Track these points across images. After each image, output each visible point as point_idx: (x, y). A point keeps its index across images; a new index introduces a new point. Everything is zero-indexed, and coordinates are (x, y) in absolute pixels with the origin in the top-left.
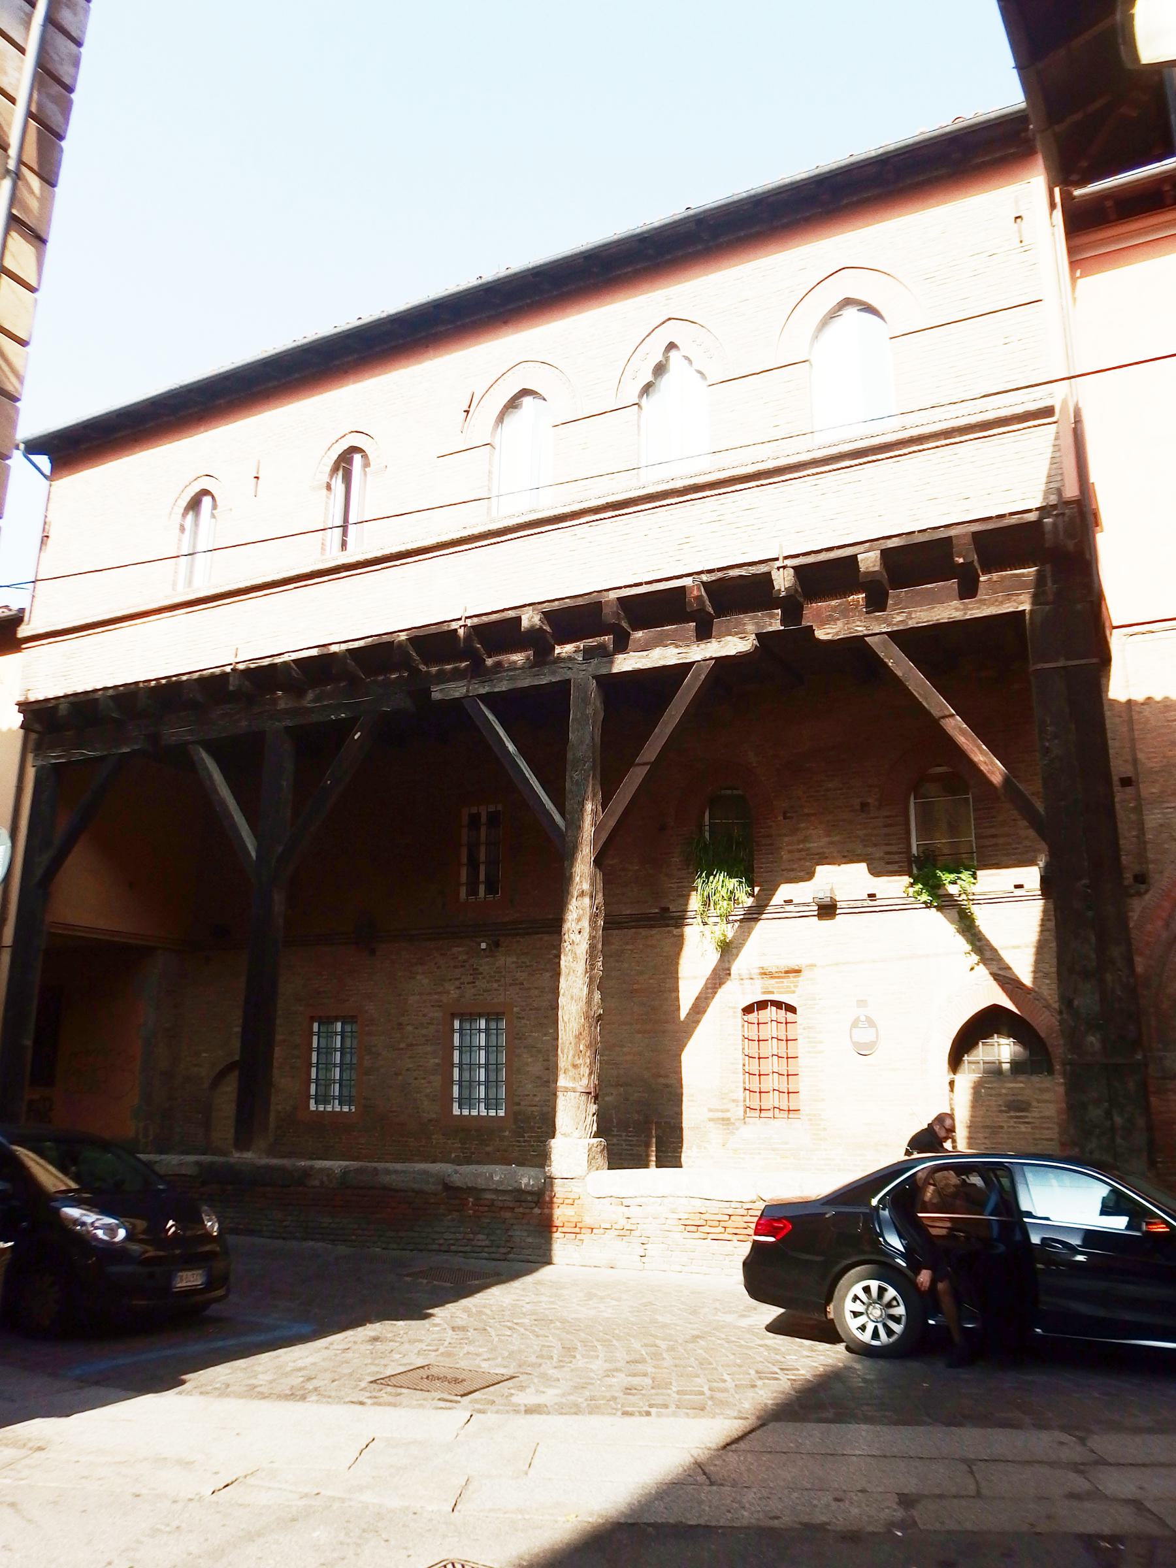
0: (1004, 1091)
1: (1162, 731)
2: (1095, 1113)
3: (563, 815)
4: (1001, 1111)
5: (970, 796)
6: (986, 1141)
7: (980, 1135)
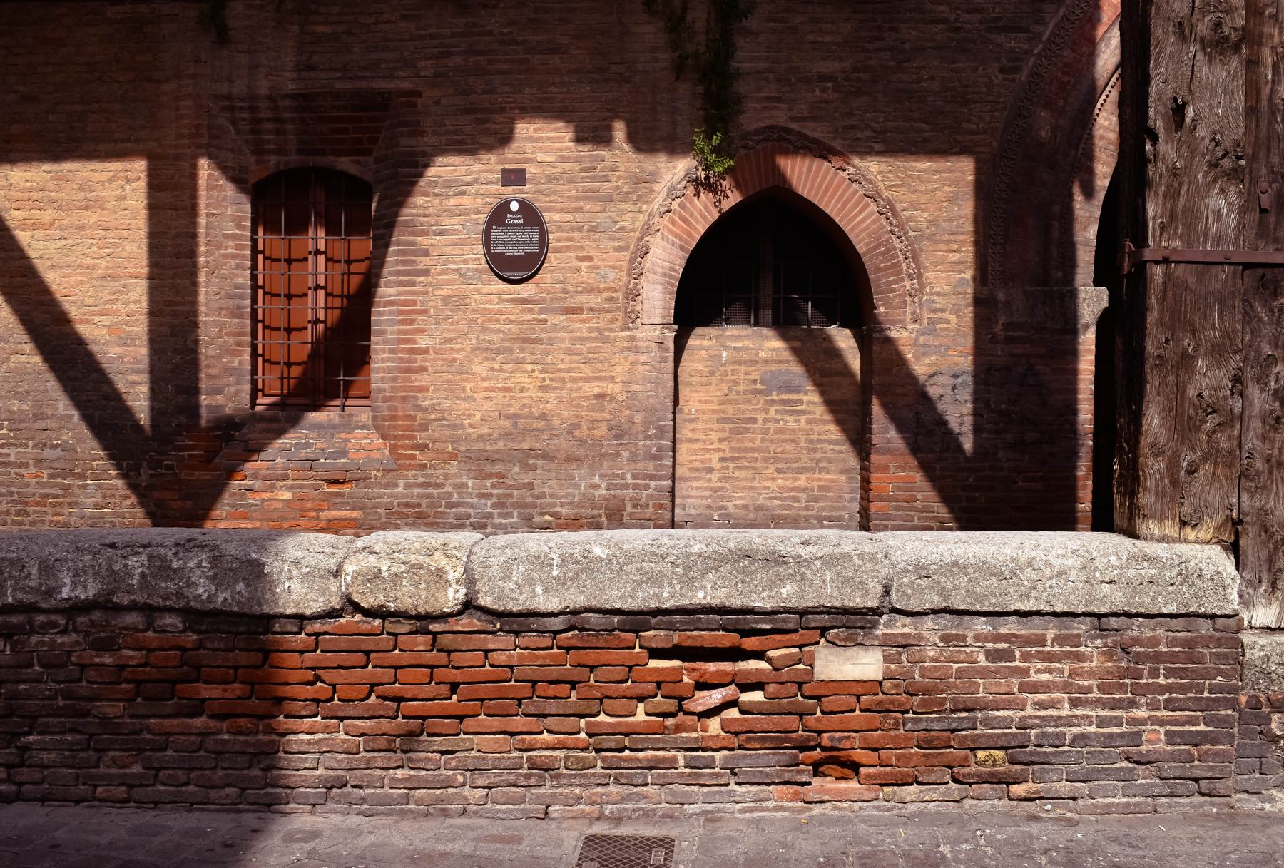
0: (763, 355)
4: (756, 392)
6: (724, 446)
7: (714, 436)
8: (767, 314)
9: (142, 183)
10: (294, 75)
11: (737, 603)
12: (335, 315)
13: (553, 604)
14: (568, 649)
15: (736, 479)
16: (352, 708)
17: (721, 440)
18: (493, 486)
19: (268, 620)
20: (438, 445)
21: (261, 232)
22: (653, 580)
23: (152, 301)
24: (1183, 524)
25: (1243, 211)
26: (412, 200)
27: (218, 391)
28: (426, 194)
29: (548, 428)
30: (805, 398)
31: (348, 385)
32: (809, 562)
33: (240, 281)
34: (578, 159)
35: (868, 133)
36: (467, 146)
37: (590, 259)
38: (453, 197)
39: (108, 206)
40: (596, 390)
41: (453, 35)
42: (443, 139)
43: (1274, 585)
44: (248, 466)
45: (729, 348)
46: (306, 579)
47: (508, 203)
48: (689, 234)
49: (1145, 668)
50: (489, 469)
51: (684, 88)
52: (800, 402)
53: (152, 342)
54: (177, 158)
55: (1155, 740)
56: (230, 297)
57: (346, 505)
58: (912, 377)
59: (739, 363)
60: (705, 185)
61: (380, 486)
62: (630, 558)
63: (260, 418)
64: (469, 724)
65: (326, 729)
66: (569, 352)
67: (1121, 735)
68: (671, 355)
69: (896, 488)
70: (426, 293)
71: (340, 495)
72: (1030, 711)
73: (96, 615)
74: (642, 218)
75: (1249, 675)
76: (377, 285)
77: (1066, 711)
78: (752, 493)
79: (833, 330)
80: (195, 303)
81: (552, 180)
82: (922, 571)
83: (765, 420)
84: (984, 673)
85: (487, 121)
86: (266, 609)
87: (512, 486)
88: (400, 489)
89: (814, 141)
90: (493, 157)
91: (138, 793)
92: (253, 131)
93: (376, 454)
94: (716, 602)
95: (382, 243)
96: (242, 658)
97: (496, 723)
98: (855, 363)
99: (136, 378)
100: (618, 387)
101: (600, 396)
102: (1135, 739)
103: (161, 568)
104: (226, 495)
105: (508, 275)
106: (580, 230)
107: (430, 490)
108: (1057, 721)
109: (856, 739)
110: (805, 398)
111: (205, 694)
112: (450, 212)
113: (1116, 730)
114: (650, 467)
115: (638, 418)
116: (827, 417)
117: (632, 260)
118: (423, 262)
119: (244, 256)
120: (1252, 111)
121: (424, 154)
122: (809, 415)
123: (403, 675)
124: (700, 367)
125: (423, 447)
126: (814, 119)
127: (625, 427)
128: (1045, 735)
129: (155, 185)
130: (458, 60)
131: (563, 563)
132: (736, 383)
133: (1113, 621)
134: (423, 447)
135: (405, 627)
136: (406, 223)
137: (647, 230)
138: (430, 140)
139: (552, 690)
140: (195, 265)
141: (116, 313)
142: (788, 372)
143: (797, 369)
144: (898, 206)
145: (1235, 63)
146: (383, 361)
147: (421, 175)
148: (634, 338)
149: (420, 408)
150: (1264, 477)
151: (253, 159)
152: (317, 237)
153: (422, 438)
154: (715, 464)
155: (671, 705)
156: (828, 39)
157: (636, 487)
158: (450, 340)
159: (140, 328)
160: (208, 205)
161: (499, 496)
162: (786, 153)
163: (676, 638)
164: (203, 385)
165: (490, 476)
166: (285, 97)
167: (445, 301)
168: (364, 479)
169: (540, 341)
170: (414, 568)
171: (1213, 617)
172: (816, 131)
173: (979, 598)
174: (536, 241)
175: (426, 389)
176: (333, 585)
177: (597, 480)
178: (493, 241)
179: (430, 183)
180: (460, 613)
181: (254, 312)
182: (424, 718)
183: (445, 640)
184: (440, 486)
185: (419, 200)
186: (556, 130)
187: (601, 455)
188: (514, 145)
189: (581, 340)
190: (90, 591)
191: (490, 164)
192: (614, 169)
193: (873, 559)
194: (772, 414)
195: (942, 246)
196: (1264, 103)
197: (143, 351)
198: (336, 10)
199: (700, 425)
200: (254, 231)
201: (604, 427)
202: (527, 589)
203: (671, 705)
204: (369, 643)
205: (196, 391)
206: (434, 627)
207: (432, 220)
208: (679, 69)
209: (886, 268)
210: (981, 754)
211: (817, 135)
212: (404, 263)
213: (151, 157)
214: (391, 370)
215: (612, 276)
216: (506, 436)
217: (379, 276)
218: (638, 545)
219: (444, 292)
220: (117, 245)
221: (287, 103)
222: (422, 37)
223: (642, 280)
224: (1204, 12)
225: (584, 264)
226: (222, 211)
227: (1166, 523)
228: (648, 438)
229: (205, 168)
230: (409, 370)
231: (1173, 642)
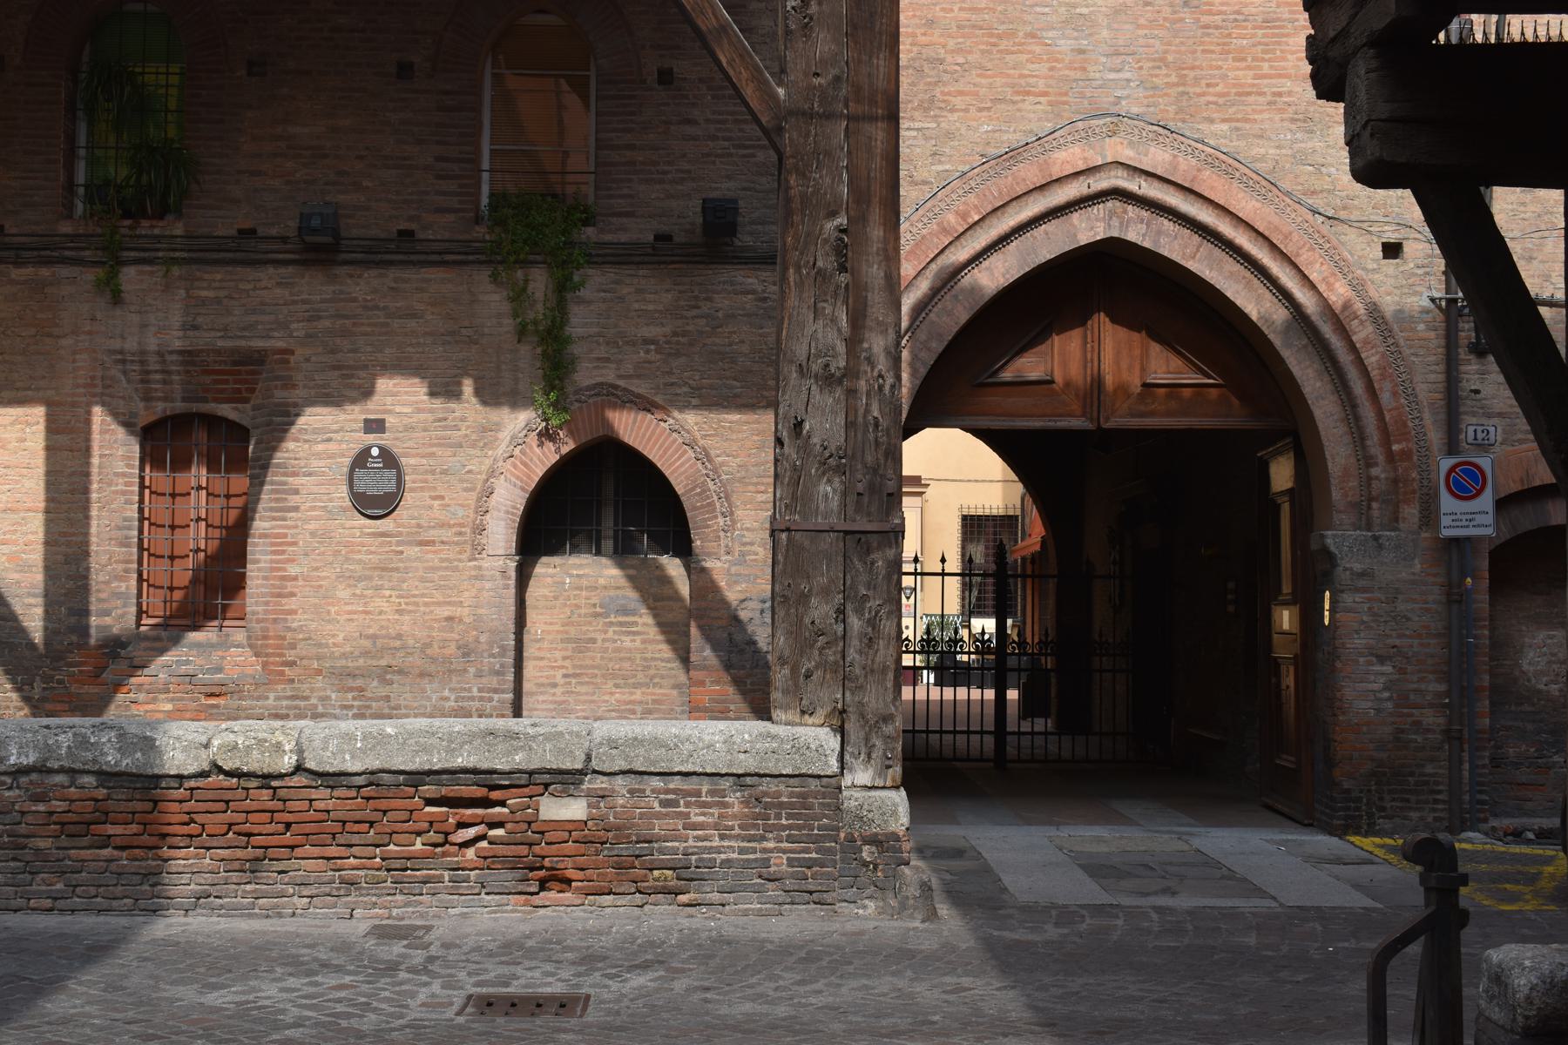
0: (602, 581)
2: (820, 611)
4: (596, 615)
5: (592, 73)
6: (567, 663)
7: (558, 654)
8: (608, 545)
9: (41, 427)
10: (181, 334)
11: (485, 766)
12: (214, 545)
13: (357, 767)
14: (368, 799)
15: (578, 693)
16: (214, 842)
17: (565, 658)
18: (354, 699)
19: (153, 781)
20: (305, 662)
21: (148, 470)
22: (425, 749)
23: (47, 532)
24: (803, 712)
25: (844, 494)
26: (284, 445)
27: (107, 613)
28: (297, 440)
29: (403, 647)
30: (640, 620)
31: (225, 608)
32: (534, 737)
33: (129, 514)
34: (431, 411)
35: (685, 389)
36: (332, 398)
37: (442, 498)
38: (319, 446)
39: (10, 446)
40: (446, 614)
41: (323, 301)
42: (313, 392)
43: (869, 756)
44: (133, 680)
45: (571, 576)
46: (185, 749)
47: (369, 448)
48: (529, 477)
49: (772, 812)
50: (351, 683)
51: (525, 349)
52: (636, 624)
53: (47, 568)
54: (74, 405)
55: (780, 863)
56: (119, 528)
57: (215, 698)
58: (725, 603)
59: (580, 589)
60: (546, 435)
61: (252, 698)
62: (411, 734)
63: (146, 638)
64: (298, 852)
65: (197, 856)
66: (422, 580)
67: (756, 860)
68: (512, 582)
69: (712, 700)
70: (296, 527)
71: (216, 706)
72: (691, 842)
73: (34, 776)
74: (488, 462)
75: (847, 819)
76: (253, 519)
77: (716, 843)
78: (592, 706)
79: (665, 560)
80: (87, 534)
81: (409, 428)
82: (613, 744)
83: (604, 640)
84: (659, 816)
85: (352, 376)
86: (156, 771)
87: (370, 699)
88: (270, 701)
89: (639, 396)
90: (357, 408)
91: (60, 904)
92: (142, 381)
93: (249, 671)
94: (470, 765)
95: (258, 482)
96: (139, 806)
97: (317, 851)
98: (684, 589)
99: (32, 601)
100: (466, 610)
101: (450, 619)
102: (766, 863)
103: (82, 742)
104: (113, 707)
105: (369, 512)
106: (433, 472)
107: (297, 702)
108: (710, 850)
109: (569, 862)
110: (640, 620)
111: (111, 832)
112: (318, 456)
113: (752, 856)
114: (494, 682)
115: (483, 638)
116: (660, 637)
117: (479, 499)
118: (293, 500)
119: (132, 492)
120: (850, 425)
121: (296, 405)
122: (642, 636)
123: (253, 817)
124: (546, 592)
125: (292, 664)
126: (639, 377)
127: (472, 646)
128: (701, 860)
129: (53, 428)
130: (327, 323)
131: (364, 738)
132: (578, 607)
133: (748, 780)
134: (292, 664)
135: (254, 783)
136: (278, 466)
137: (492, 473)
138: (299, 394)
139: (356, 827)
140: (88, 500)
141: (15, 543)
142: (624, 597)
143: (632, 594)
144: (712, 453)
145: (839, 392)
146: (257, 587)
147: (292, 423)
148: (480, 568)
149: (289, 629)
150: (861, 680)
151: (141, 405)
152: (199, 474)
153: (290, 655)
154: (559, 680)
155: (440, 838)
156: (651, 307)
157: (481, 699)
158: (317, 569)
159: (36, 556)
160: (101, 447)
161: (359, 708)
162: (614, 406)
163: (444, 791)
164: (93, 608)
165: (351, 689)
166: (171, 352)
167: (313, 534)
168: (237, 692)
169: (397, 569)
170: (261, 742)
171: (819, 777)
172: (641, 388)
173: (653, 763)
174: (394, 482)
175: (294, 612)
176: (203, 754)
177: (446, 693)
178: (356, 482)
179: (300, 430)
180: (293, 774)
181: (141, 541)
182: (266, 848)
183: (282, 793)
184: (307, 698)
185: (290, 445)
186: (412, 385)
187: (450, 671)
188: (376, 398)
189: (434, 569)
190: (31, 759)
191: (354, 415)
192: (463, 419)
193: (578, 735)
194: (610, 634)
195: (751, 488)
196: (860, 419)
197: (39, 577)
198: (219, 277)
199: (546, 645)
200: (142, 469)
201: (453, 646)
202: (339, 757)
203: (440, 838)
204: (228, 795)
205: (86, 613)
206: (274, 783)
207: (302, 463)
208: (521, 333)
209: (702, 507)
210: (656, 873)
211: (640, 391)
212: (277, 500)
213: (49, 404)
214: (264, 595)
215: (461, 513)
216: (366, 653)
217: (254, 511)
218: (417, 726)
219: (312, 526)
220: (17, 482)
221: (174, 357)
222: (294, 302)
223: (488, 516)
224: (818, 356)
225: (436, 503)
226: (114, 452)
227: (790, 712)
228: (493, 656)
229: (98, 414)
230: (280, 595)
231: (791, 795)
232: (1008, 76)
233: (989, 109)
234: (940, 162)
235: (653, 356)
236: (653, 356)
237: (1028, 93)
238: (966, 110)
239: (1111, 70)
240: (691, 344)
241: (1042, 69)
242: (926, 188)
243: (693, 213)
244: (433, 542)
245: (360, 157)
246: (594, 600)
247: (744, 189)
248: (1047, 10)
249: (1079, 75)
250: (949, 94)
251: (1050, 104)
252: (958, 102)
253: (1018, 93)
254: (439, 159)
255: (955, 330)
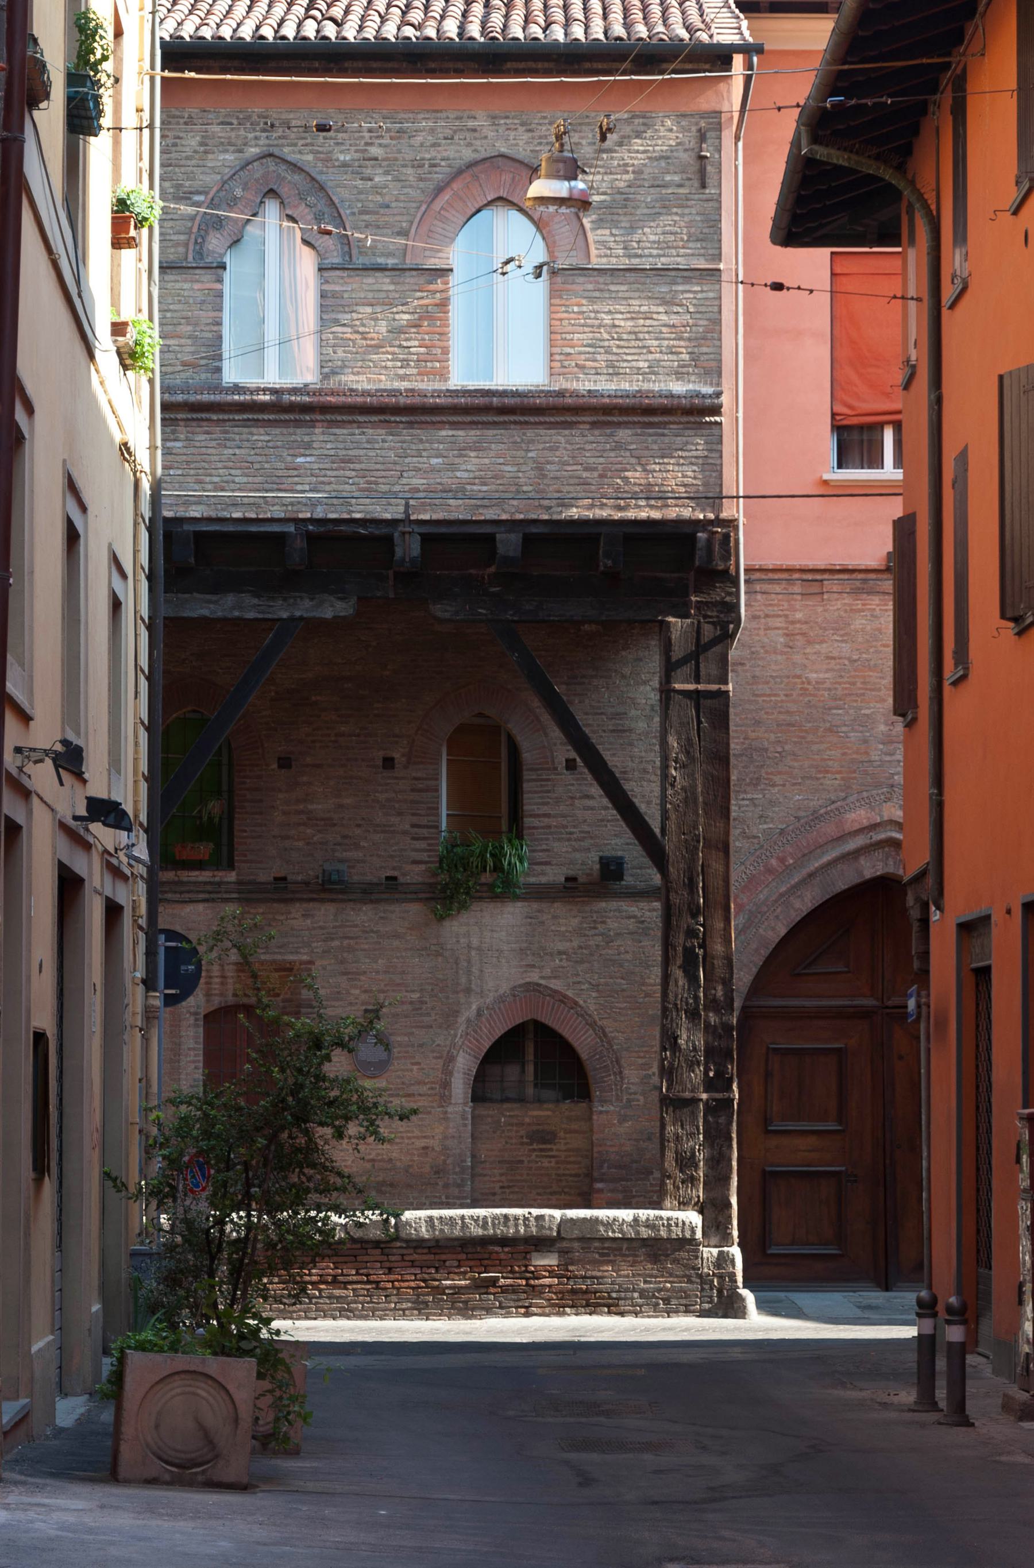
0: (527, 1120)
1: (747, 706)
3: (922, 1252)
6: (503, 1178)
17: (501, 1175)
33: (197, 1076)
37: (418, 1064)
40: (423, 1145)
45: (505, 1116)
48: (479, 1049)
56: (192, 1086)
59: (512, 1125)
85: (356, 979)
101: (425, 1148)
106: (413, 1046)
119: (199, 1061)
126: (555, 978)
132: (510, 1138)
144: (607, 1030)
154: (498, 1190)
156: (563, 929)
195: (634, 1054)
198: (261, 910)
206: (382, 1246)
209: (601, 1068)
222: (314, 928)
225: (415, 1067)
228: (455, 1173)
232: (814, 760)
233: (799, 784)
234: (765, 823)
235: (564, 963)
236: (564, 963)
237: (827, 772)
238: (784, 785)
239: (886, 754)
240: (592, 955)
241: (836, 753)
242: (756, 841)
243: (593, 859)
244: (414, 1095)
245: (359, 826)
246: (522, 1133)
247: (627, 844)
248: (840, 711)
249: (864, 758)
250: (772, 773)
251: (843, 779)
252: (778, 779)
253: (820, 772)
254: (413, 826)
255: (777, 941)
